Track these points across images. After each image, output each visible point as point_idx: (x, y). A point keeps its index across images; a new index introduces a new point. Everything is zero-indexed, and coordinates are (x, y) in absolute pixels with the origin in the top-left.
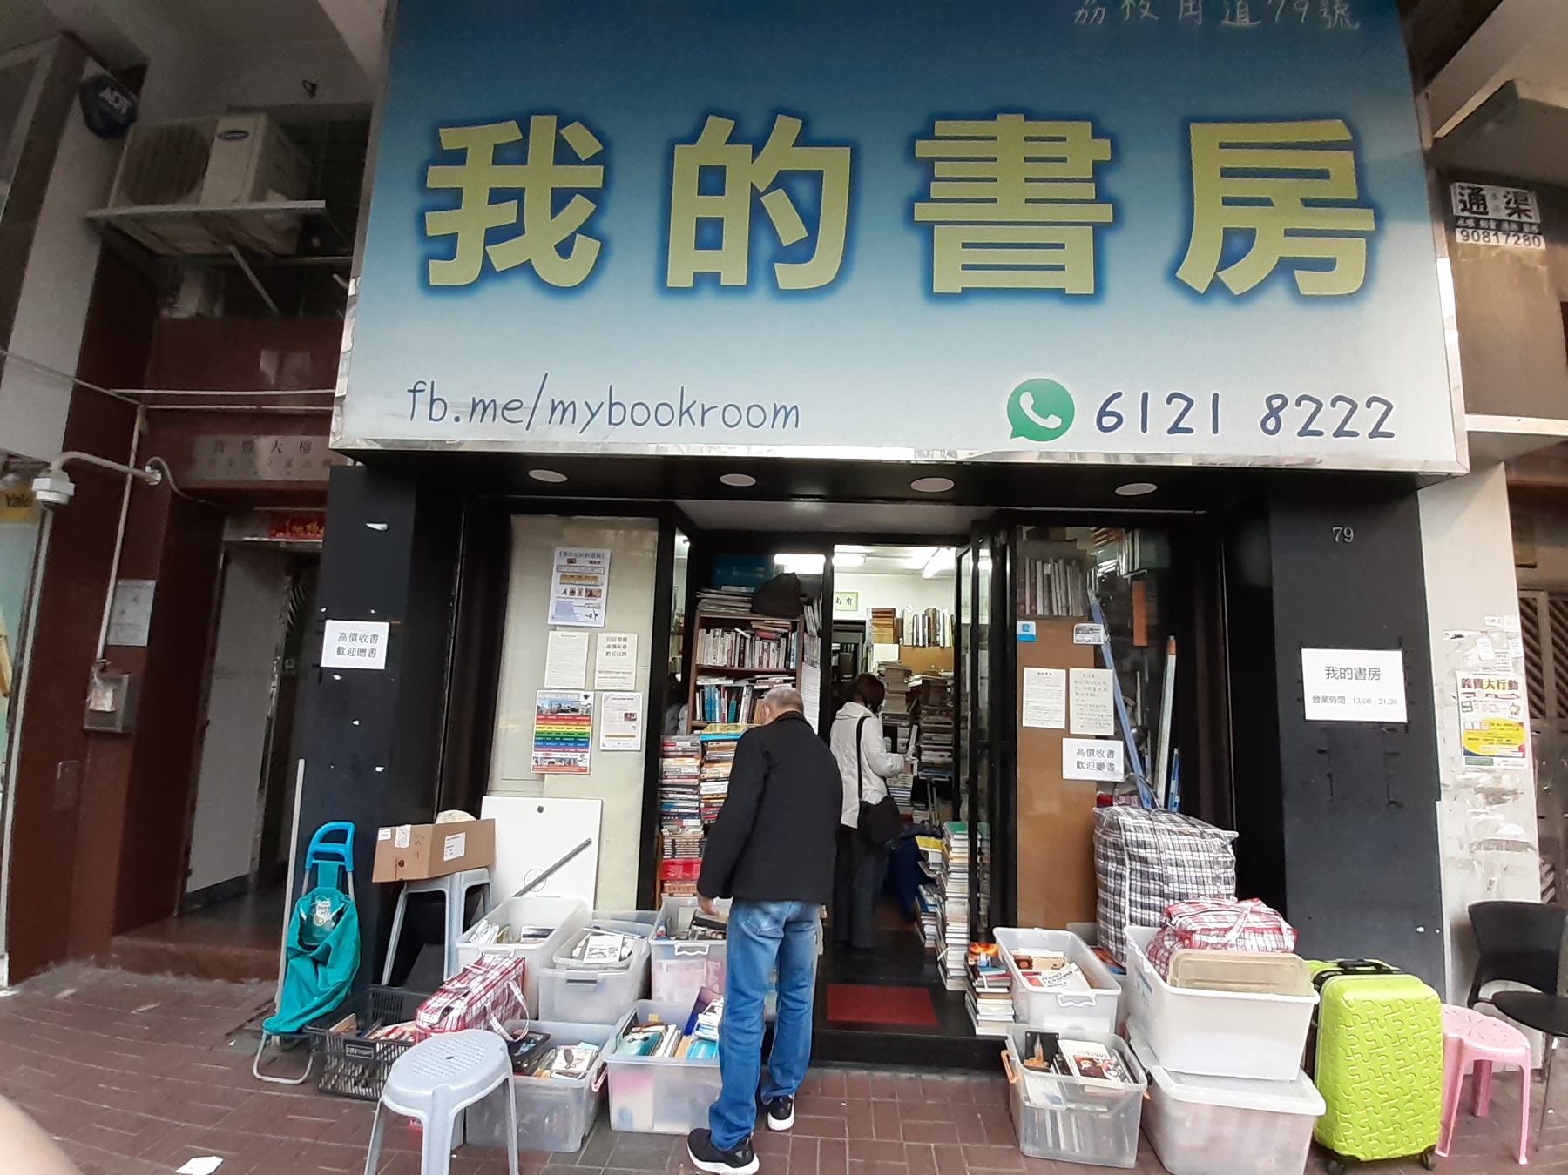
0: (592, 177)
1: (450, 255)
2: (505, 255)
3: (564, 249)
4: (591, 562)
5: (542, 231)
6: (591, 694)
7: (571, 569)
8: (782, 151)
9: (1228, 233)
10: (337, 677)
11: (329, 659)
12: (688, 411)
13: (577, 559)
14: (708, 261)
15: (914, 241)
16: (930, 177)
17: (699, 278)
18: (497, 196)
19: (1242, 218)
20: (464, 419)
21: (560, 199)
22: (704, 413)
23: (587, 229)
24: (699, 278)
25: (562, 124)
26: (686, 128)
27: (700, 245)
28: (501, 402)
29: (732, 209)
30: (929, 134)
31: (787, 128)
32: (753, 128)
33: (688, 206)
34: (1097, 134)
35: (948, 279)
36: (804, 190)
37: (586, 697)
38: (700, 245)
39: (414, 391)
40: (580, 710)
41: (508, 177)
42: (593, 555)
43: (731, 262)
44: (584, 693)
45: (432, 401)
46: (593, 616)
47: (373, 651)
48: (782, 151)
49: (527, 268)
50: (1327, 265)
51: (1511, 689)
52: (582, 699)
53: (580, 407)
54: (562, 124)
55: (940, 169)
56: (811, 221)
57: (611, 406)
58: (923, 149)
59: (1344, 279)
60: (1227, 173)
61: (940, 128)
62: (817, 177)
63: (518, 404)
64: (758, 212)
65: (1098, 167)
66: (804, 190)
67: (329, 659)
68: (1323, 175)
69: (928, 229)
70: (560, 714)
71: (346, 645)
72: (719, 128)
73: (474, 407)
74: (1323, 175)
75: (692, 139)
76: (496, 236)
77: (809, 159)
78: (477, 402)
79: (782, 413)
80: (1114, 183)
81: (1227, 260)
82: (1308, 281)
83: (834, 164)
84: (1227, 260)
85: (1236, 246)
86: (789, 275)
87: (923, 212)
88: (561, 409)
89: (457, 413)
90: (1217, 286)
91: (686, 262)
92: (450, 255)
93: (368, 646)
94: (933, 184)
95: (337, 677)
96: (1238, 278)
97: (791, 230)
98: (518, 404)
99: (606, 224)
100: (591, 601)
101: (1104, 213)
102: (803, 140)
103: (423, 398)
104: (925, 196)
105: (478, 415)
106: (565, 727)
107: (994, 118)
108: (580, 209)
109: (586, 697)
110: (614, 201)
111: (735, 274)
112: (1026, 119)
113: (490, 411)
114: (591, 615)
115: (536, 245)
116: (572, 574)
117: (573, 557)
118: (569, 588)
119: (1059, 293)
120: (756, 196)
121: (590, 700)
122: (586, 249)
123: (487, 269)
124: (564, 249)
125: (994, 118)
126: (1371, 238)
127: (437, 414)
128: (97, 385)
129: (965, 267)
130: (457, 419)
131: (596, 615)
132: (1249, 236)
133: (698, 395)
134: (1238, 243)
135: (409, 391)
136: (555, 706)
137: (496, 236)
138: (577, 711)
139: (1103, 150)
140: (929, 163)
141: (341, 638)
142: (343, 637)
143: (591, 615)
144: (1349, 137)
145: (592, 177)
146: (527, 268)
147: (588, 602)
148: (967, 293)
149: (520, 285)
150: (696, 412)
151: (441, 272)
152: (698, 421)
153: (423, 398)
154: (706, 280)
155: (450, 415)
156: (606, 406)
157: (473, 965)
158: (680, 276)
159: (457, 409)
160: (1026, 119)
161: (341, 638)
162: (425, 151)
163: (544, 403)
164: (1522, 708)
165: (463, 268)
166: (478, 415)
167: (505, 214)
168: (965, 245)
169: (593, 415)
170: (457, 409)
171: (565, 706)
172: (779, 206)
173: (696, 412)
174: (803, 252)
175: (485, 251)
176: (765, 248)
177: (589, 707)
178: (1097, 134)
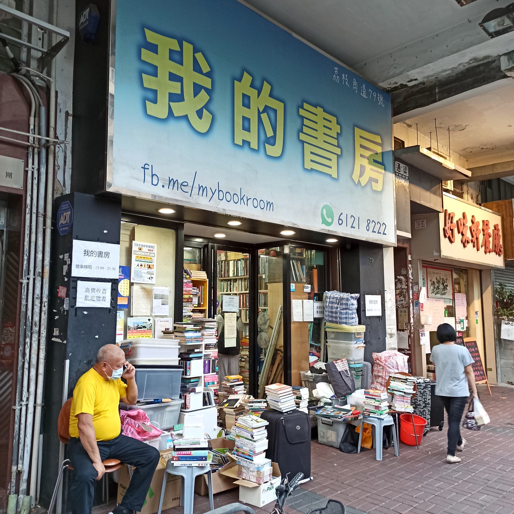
2: (178, 109)
4: (149, 250)
6: (151, 318)
7: (140, 253)
10: (85, 313)
11: (80, 303)
13: (143, 248)
14: (247, 136)
15: (300, 145)
20: (166, 187)
22: (247, 200)
23: (206, 107)
28: (180, 182)
33: (240, 111)
37: (149, 320)
39: (144, 168)
40: (147, 327)
42: (150, 247)
43: (252, 138)
44: (148, 318)
45: (153, 175)
46: (151, 278)
47: (104, 297)
49: (186, 117)
51: (264, 307)
52: (148, 321)
53: (209, 190)
57: (219, 191)
67: (80, 303)
69: (303, 142)
70: (138, 330)
71: (90, 295)
73: (170, 182)
78: (170, 180)
89: (164, 183)
91: (241, 135)
93: (101, 295)
95: (85, 313)
97: (270, 134)
98: (186, 184)
99: (212, 107)
100: (149, 270)
103: (148, 172)
105: (171, 187)
106: (132, 337)
108: (203, 95)
109: (149, 320)
110: (216, 96)
113: (176, 185)
114: (150, 278)
116: (144, 256)
117: (141, 247)
118: (140, 263)
121: (151, 322)
127: (155, 182)
128: (21, 140)
131: (152, 278)
135: (142, 167)
136: (136, 325)
138: (146, 327)
141: (86, 291)
142: (87, 290)
143: (150, 278)
144: (381, 142)
145: (206, 82)
146: (186, 117)
147: (148, 271)
148: (312, 170)
149: (183, 124)
152: (246, 203)
153: (148, 172)
155: (160, 184)
156: (217, 191)
157: (330, 397)
159: (164, 182)
161: (86, 291)
164: (260, 318)
166: (171, 187)
167: (175, 88)
169: (213, 194)
170: (164, 182)
171: (140, 325)
174: (271, 141)
177: (151, 325)
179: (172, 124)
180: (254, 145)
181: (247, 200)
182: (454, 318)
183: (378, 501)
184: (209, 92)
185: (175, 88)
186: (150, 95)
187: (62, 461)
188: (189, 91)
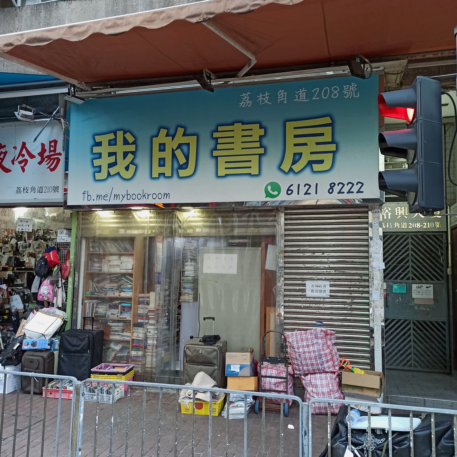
0: (132, 148)
1: (100, 172)
2: (113, 171)
3: (127, 168)
5: (122, 163)
8: (180, 139)
9: (295, 154)
12: (144, 195)
14: (162, 170)
15: (213, 162)
16: (217, 143)
17: (160, 174)
18: (110, 154)
19: (298, 149)
21: (125, 154)
22: (148, 196)
23: (132, 163)
24: (160, 174)
25: (125, 133)
26: (154, 132)
27: (160, 166)
29: (167, 155)
30: (217, 131)
31: (181, 131)
32: (172, 132)
33: (157, 155)
34: (261, 127)
35: (222, 172)
36: (185, 148)
38: (160, 166)
39: (84, 193)
41: (112, 149)
43: (167, 170)
45: (88, 196)
48: (180, 139)
49: (118, 174)
50: (321, 162)
53: (121, 196)
54: (125, 133)
55: (220, 141)
56: (187, 157)
57: (127, 195)
58: (216, 135)
59: (326, 166)
60: (296, 136)
61: (220, 128)
62: (188, 144)
63: (107, 196)
64: (174, 156)
65: (261, 137)
66: (185, 148)
68: (322, 135)
69: (216, 157)
72: (163, 132)
73: (97, 197)
74: (322, 135)
75: (157, 136)
76: (111, 165)
77: (185, 140)
79: (166, 195)
80: (265, 141)
81: (294, 162)
82: (316, 167)
83: (192, 140)
84: (294, 162)
85: (297, 157)
86: (182, 173)
87: (215, 153)
88: (116, 196)
90: (291, 170)
91: (157, 170)
92: (100, 172)
94: (218, 145)
96: (296, 168)
97: (182, 160)
98: (107, 196)
101: (262, 151)
102: (184, 135)
103: (86, 195)
104: (216, 149)
107: (234, 125)
108: (130, 157)
110: (139, 154)
111: (168, 174)
112: (242, 124)
115: (120, 168)
119: (250, 174)
120: (173, 151)
122: (132, 167)
123: (109, 175)
124: (127, 168)
125: (234, 125)
126: (334, 153)
129: (226, 168)
130: (94, 200)
132: (301, 154)
133: (147, 191)
134: (297, 157)
137: (111, 165)
139: (262, 132)
140: (217, 139)
146: (118, 174)
148: (226, 175)
150: (146, 196)
151: (98, 176)
152: (147, 198)
154: (162, 175)
156: (126, 195)
158: (155, 175)
160: (242, 124)
162: (91, 142)
163: (113, 196)
165: (103, 174)
167: (112, 160)
168: (226, 162)
169: (123, 197)
172: (178, 153)
173: (146, 196)
174: (184, 166)
175: (108, 170)
176: (176, 166)
178: (261, 127)
179: (110, 180)
180: (168, 174)
181: (148, 196)
182: (253, 389)
183: (446, 241)
184: (133, 153)
185: (112, 159)
186: (97, 169)
187: (412, 445)
188: (120, 156)
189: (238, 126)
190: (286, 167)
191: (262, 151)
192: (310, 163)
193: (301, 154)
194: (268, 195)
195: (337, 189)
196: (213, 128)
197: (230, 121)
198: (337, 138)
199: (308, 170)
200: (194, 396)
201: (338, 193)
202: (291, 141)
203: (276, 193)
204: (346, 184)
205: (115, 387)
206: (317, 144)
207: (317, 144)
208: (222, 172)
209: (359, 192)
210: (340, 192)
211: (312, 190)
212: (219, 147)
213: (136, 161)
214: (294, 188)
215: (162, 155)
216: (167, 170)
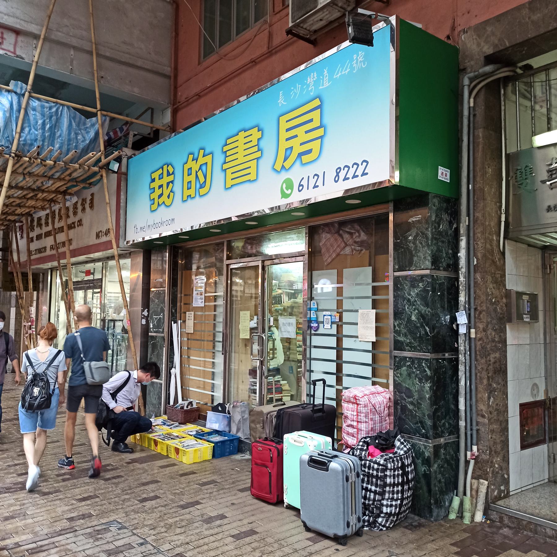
2: (161, 201)
23: (171, 191)
32: (196, 156)
56: (205, 177)
61: (229, 141)
66: (204, 168)
81: (286, 159)
82: (305, 158)
86: (203, 191)
90: (283, 167)
96: (287, 164)
120: (197, 172)
132: (291, 148)
134: (161, 176)
189: (242, 134)
190: (278, 167)
191: (258, 154)
192: (300, 155)
193: (291, 148)
194: (285, 195)
195: (342, 175)
196: (223, 143)
197: (235, 132)
198: (326, 121)
199: (298, 163)
200: (357, 418)
201: (344, 180)
202: (284, 135)
203: (289, 192)
204: (360, 164)
205: (24, 515)
206: (307, 132)
207: (307, 132)
208: (229, 183)
209: (364, 174)
210: (346, 179)
211: (320, 183)
212: (228, 159)
213: (174, 189)
214: (304, 183)
215: (187, 179)
216: (192, 192)
